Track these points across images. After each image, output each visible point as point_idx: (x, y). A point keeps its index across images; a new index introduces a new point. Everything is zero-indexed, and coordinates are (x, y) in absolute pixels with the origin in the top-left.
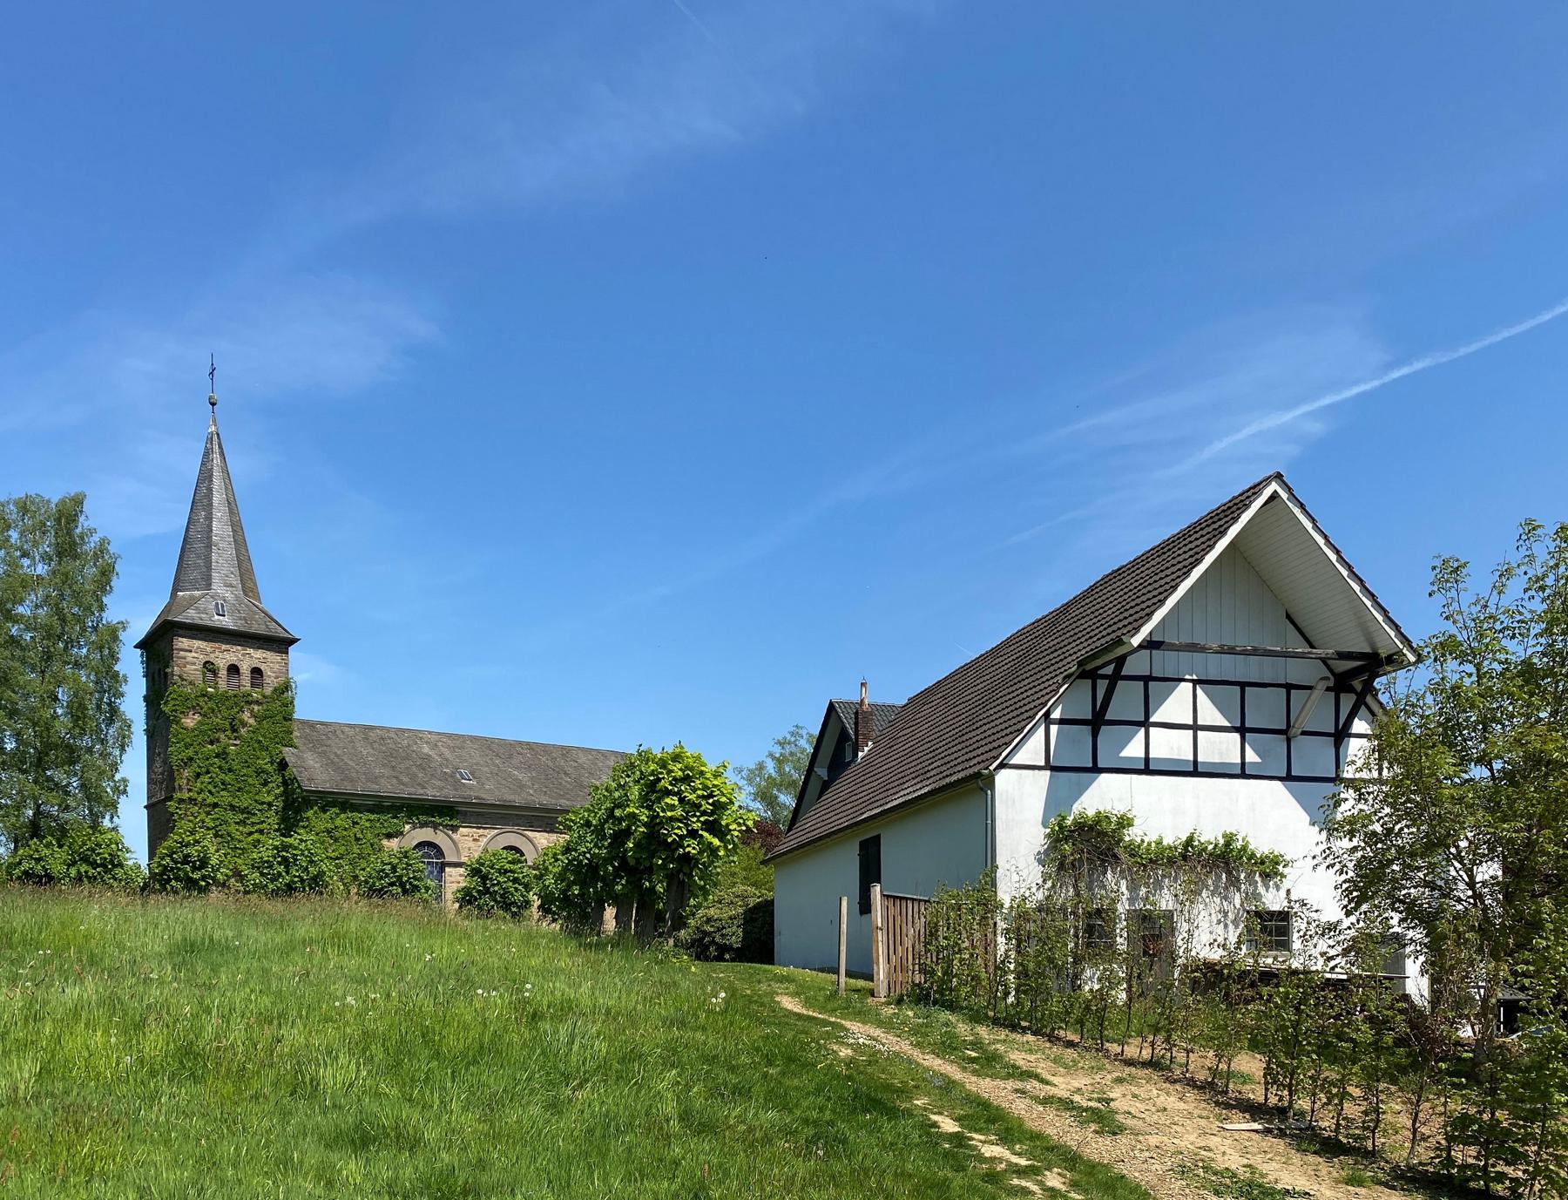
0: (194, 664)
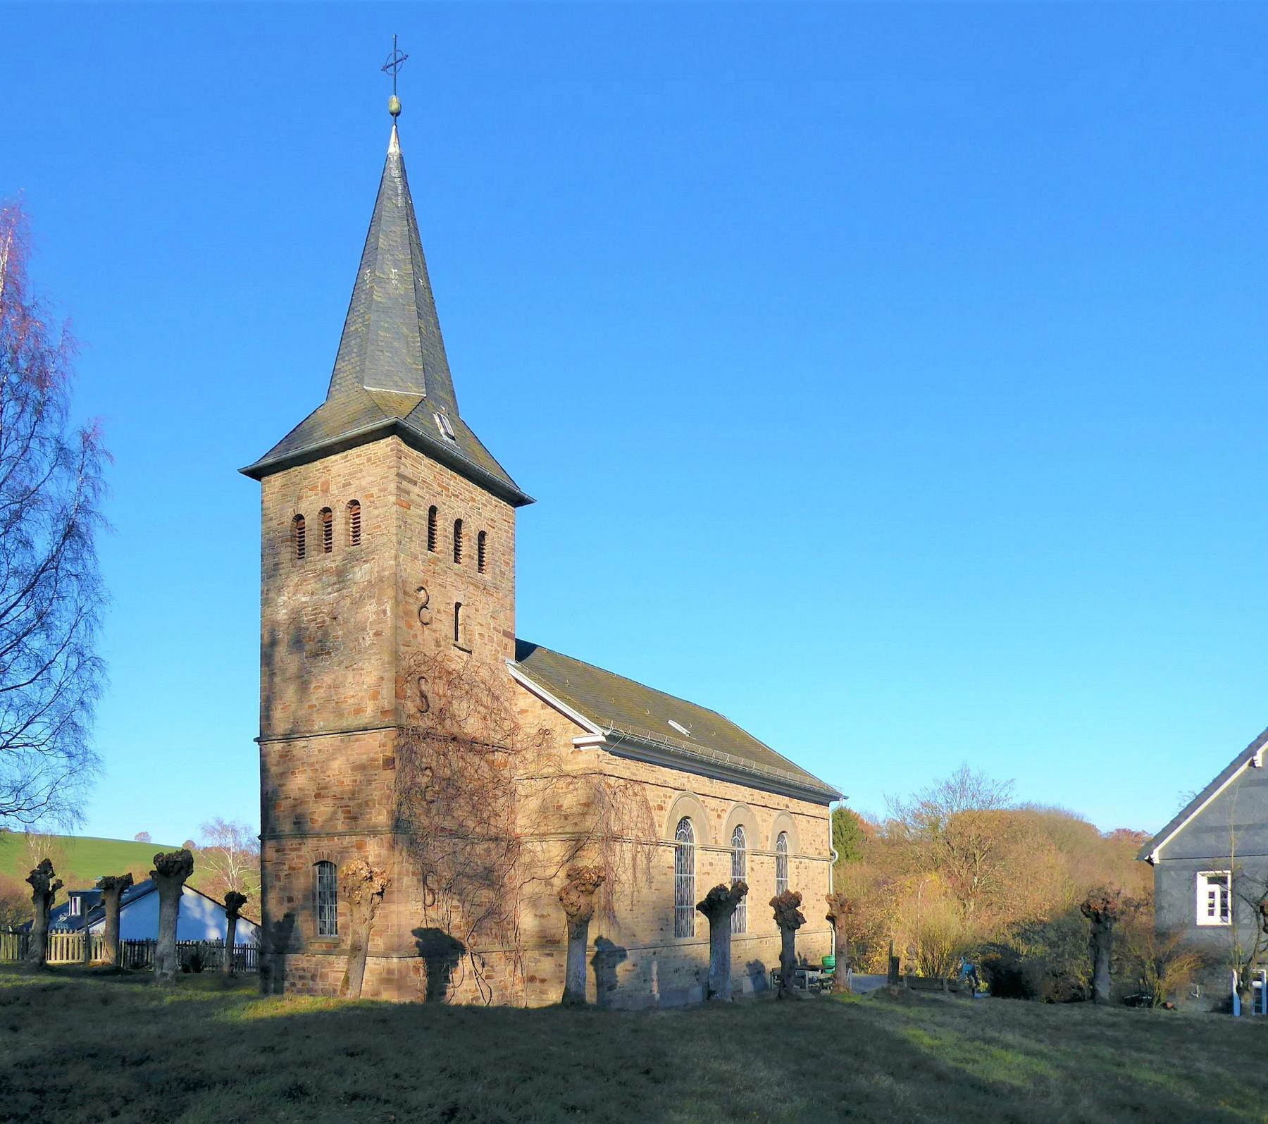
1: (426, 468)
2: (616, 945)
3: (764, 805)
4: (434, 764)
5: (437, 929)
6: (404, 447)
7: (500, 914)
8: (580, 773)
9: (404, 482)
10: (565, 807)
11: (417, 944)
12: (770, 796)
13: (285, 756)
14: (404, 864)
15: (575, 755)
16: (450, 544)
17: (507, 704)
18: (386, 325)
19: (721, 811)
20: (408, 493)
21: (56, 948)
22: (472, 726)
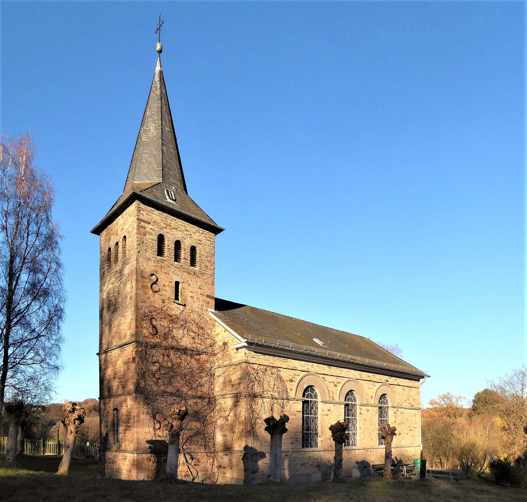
1: (156, 215)
2: (259, 451)
3: (369, 380)
4: (161, 361)
5: (162, 440)
6: (142, 206)
7: (204, 434)
8: (237, 363)
9: (142, 223)
10: (233, 380)
11: (150, 448)
12: (374, 375)
13: (106, 360)
14: (141, 409)
15: (236, 354)
16: (172, 253)
17: (209, 332)
18: (147, 151)
19: (337, 383)
20: (145, 228)
22: (186, 342)
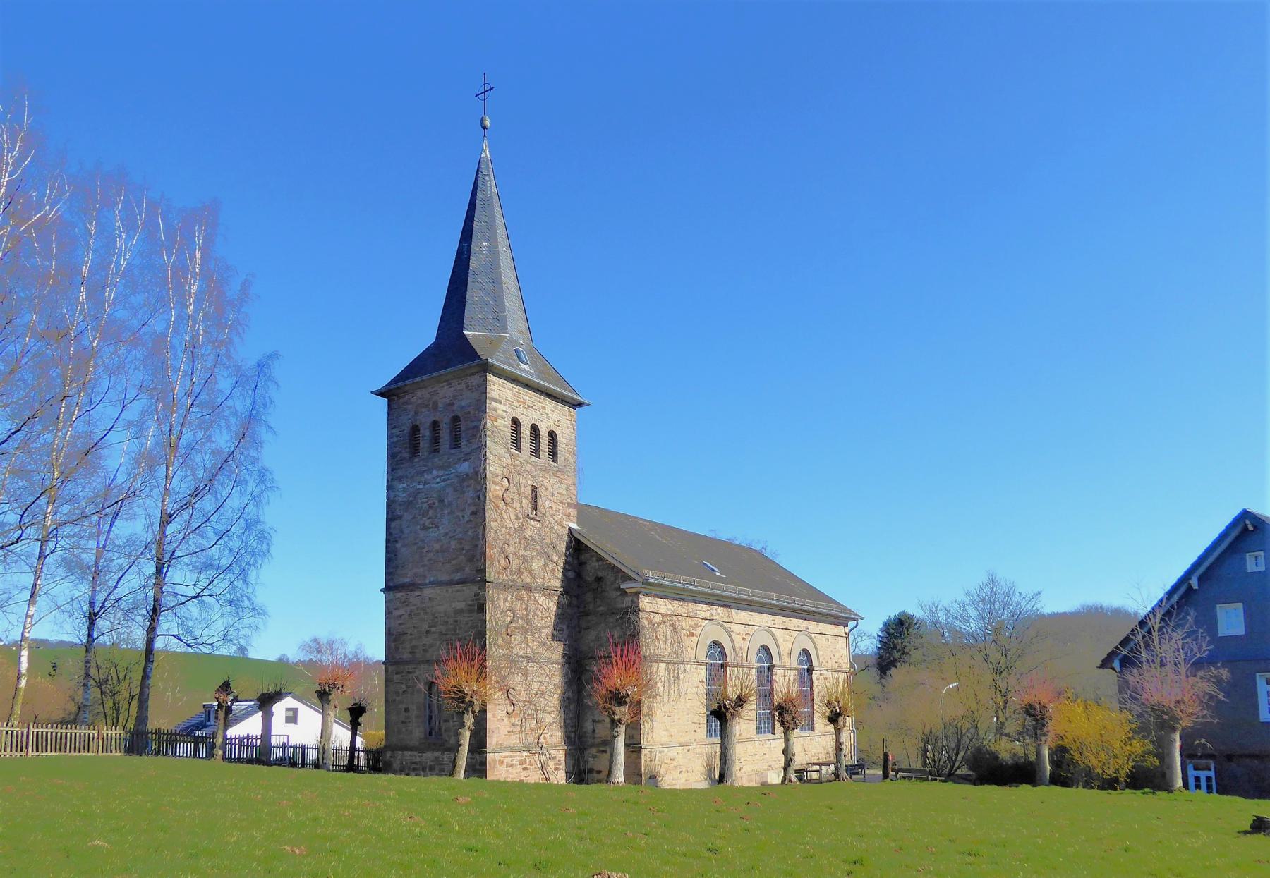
0: (503, 418)
9: (493, 403)
21: (17, 741)
